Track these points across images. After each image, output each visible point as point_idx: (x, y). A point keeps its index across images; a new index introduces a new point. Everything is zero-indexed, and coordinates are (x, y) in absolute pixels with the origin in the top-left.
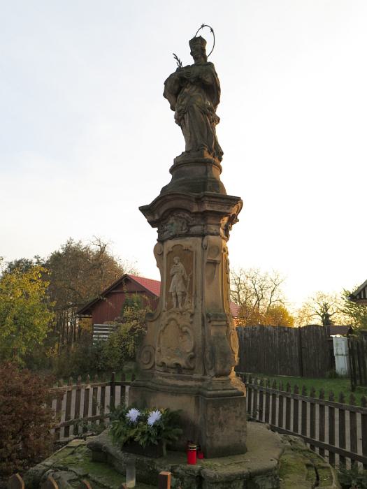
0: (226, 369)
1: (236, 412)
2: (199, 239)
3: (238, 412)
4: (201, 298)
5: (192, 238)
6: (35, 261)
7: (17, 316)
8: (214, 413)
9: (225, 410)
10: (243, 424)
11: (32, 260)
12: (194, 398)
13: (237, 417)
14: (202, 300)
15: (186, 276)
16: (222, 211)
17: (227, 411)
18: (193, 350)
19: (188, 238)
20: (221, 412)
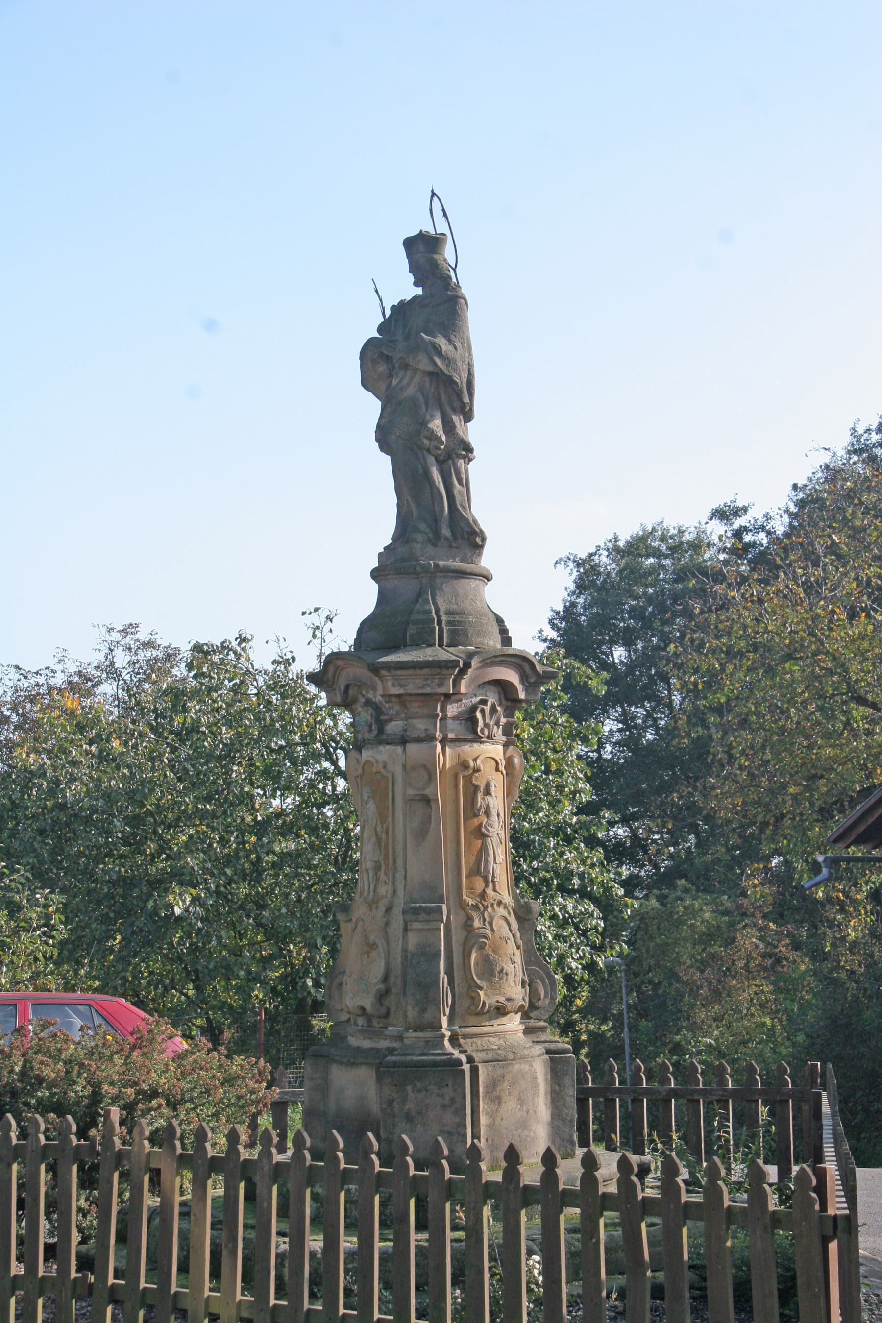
0: (428, 1016)
1: (442, 1096)
2: (399, 749)
3: (447, 1097)
4: (403, 873)
5: (388, 747)
6: (717, 530)
7: (413, 1113)
8: (396, 1095)
9: (419, 1091)
10: (457, 1120)
11: (700, 532)
12: (374, 1072)
13: (444, 1107)
14: (405, 877)
15: (379, 828)
16: (428, 690)
17: (424, 1093)
18: (385, 979)
19: (381, 748)
20: (411, 1095)
